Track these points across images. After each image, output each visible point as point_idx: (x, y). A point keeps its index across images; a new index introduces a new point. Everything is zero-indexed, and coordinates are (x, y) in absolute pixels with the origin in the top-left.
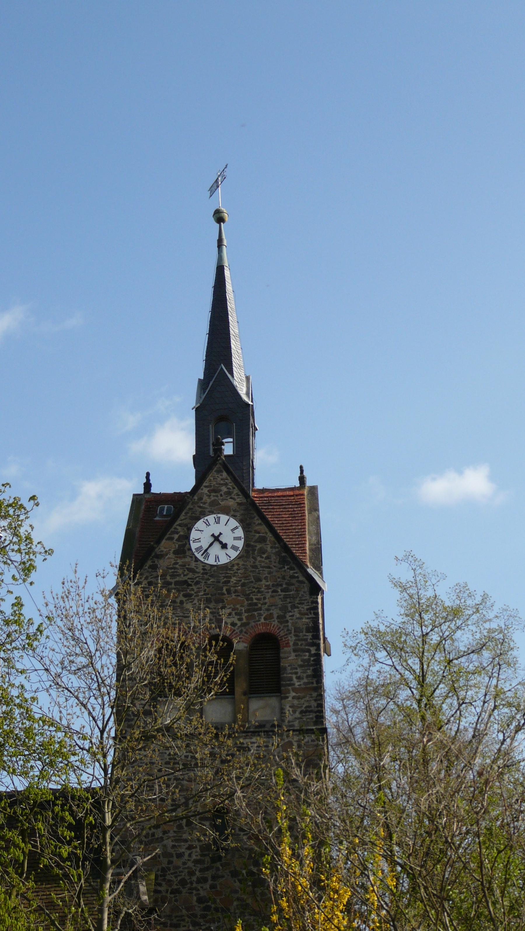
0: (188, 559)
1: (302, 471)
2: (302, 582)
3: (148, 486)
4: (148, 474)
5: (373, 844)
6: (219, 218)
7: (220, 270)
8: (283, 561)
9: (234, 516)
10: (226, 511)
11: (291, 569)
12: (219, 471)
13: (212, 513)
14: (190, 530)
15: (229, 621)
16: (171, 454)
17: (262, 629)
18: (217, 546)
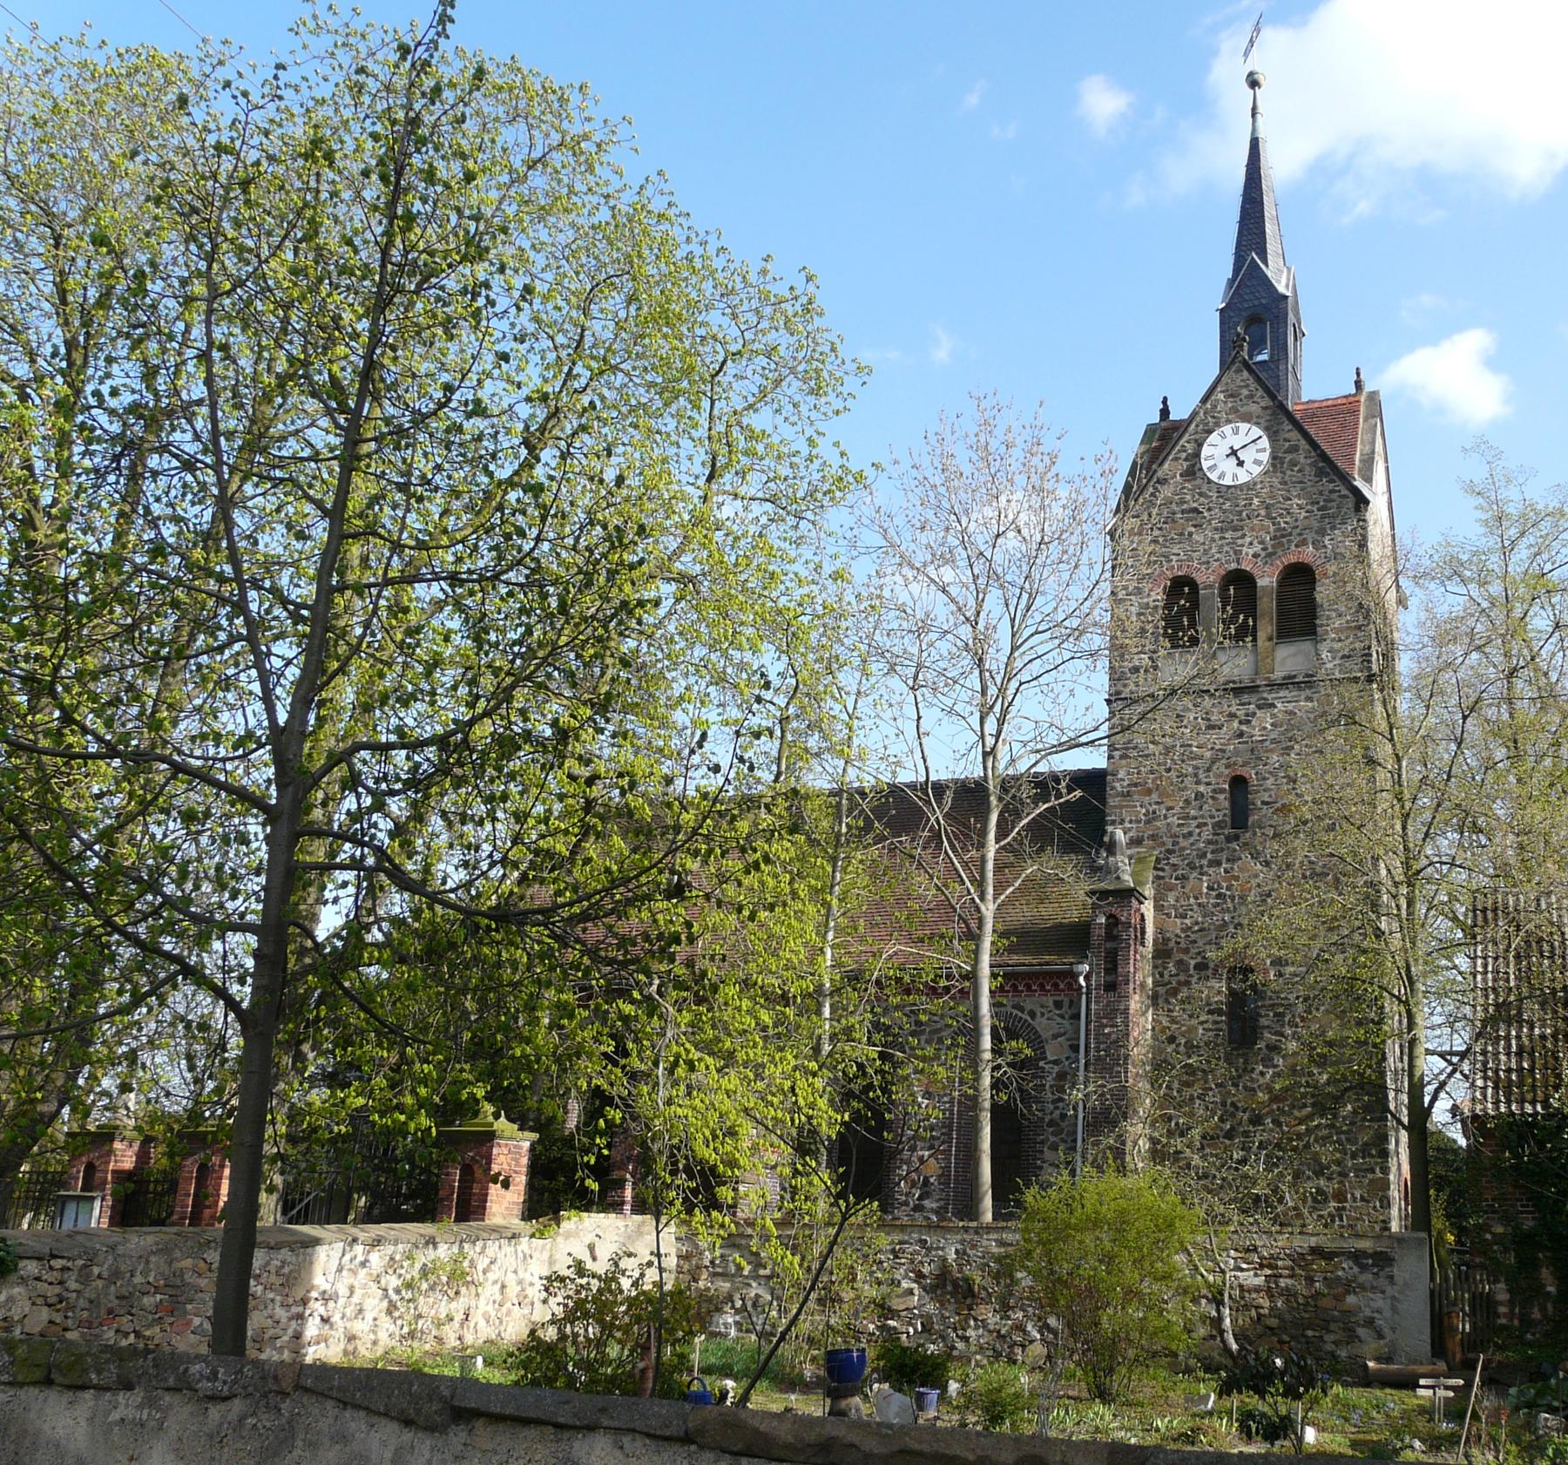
0: (1198, 482)
1: (1358, 374)
2: (1345, 497)
3: (1165, 412)
4: (1165, 401)
5: (613, 680)
6: (1253, 83)
7: (1255, 144)
8: (1320, 473)
9: (1257, 424)
10: (1246, 418)
11: (1331, 481)
12: (1238, 371)
13: (1229, 421)
14: (1200, 445)
15: (1251, 552)
16: (1189, 366)
17: (1293, 559)
18: (1233, 461)
